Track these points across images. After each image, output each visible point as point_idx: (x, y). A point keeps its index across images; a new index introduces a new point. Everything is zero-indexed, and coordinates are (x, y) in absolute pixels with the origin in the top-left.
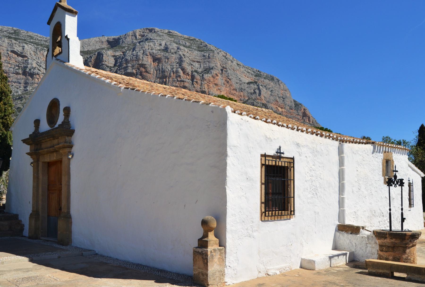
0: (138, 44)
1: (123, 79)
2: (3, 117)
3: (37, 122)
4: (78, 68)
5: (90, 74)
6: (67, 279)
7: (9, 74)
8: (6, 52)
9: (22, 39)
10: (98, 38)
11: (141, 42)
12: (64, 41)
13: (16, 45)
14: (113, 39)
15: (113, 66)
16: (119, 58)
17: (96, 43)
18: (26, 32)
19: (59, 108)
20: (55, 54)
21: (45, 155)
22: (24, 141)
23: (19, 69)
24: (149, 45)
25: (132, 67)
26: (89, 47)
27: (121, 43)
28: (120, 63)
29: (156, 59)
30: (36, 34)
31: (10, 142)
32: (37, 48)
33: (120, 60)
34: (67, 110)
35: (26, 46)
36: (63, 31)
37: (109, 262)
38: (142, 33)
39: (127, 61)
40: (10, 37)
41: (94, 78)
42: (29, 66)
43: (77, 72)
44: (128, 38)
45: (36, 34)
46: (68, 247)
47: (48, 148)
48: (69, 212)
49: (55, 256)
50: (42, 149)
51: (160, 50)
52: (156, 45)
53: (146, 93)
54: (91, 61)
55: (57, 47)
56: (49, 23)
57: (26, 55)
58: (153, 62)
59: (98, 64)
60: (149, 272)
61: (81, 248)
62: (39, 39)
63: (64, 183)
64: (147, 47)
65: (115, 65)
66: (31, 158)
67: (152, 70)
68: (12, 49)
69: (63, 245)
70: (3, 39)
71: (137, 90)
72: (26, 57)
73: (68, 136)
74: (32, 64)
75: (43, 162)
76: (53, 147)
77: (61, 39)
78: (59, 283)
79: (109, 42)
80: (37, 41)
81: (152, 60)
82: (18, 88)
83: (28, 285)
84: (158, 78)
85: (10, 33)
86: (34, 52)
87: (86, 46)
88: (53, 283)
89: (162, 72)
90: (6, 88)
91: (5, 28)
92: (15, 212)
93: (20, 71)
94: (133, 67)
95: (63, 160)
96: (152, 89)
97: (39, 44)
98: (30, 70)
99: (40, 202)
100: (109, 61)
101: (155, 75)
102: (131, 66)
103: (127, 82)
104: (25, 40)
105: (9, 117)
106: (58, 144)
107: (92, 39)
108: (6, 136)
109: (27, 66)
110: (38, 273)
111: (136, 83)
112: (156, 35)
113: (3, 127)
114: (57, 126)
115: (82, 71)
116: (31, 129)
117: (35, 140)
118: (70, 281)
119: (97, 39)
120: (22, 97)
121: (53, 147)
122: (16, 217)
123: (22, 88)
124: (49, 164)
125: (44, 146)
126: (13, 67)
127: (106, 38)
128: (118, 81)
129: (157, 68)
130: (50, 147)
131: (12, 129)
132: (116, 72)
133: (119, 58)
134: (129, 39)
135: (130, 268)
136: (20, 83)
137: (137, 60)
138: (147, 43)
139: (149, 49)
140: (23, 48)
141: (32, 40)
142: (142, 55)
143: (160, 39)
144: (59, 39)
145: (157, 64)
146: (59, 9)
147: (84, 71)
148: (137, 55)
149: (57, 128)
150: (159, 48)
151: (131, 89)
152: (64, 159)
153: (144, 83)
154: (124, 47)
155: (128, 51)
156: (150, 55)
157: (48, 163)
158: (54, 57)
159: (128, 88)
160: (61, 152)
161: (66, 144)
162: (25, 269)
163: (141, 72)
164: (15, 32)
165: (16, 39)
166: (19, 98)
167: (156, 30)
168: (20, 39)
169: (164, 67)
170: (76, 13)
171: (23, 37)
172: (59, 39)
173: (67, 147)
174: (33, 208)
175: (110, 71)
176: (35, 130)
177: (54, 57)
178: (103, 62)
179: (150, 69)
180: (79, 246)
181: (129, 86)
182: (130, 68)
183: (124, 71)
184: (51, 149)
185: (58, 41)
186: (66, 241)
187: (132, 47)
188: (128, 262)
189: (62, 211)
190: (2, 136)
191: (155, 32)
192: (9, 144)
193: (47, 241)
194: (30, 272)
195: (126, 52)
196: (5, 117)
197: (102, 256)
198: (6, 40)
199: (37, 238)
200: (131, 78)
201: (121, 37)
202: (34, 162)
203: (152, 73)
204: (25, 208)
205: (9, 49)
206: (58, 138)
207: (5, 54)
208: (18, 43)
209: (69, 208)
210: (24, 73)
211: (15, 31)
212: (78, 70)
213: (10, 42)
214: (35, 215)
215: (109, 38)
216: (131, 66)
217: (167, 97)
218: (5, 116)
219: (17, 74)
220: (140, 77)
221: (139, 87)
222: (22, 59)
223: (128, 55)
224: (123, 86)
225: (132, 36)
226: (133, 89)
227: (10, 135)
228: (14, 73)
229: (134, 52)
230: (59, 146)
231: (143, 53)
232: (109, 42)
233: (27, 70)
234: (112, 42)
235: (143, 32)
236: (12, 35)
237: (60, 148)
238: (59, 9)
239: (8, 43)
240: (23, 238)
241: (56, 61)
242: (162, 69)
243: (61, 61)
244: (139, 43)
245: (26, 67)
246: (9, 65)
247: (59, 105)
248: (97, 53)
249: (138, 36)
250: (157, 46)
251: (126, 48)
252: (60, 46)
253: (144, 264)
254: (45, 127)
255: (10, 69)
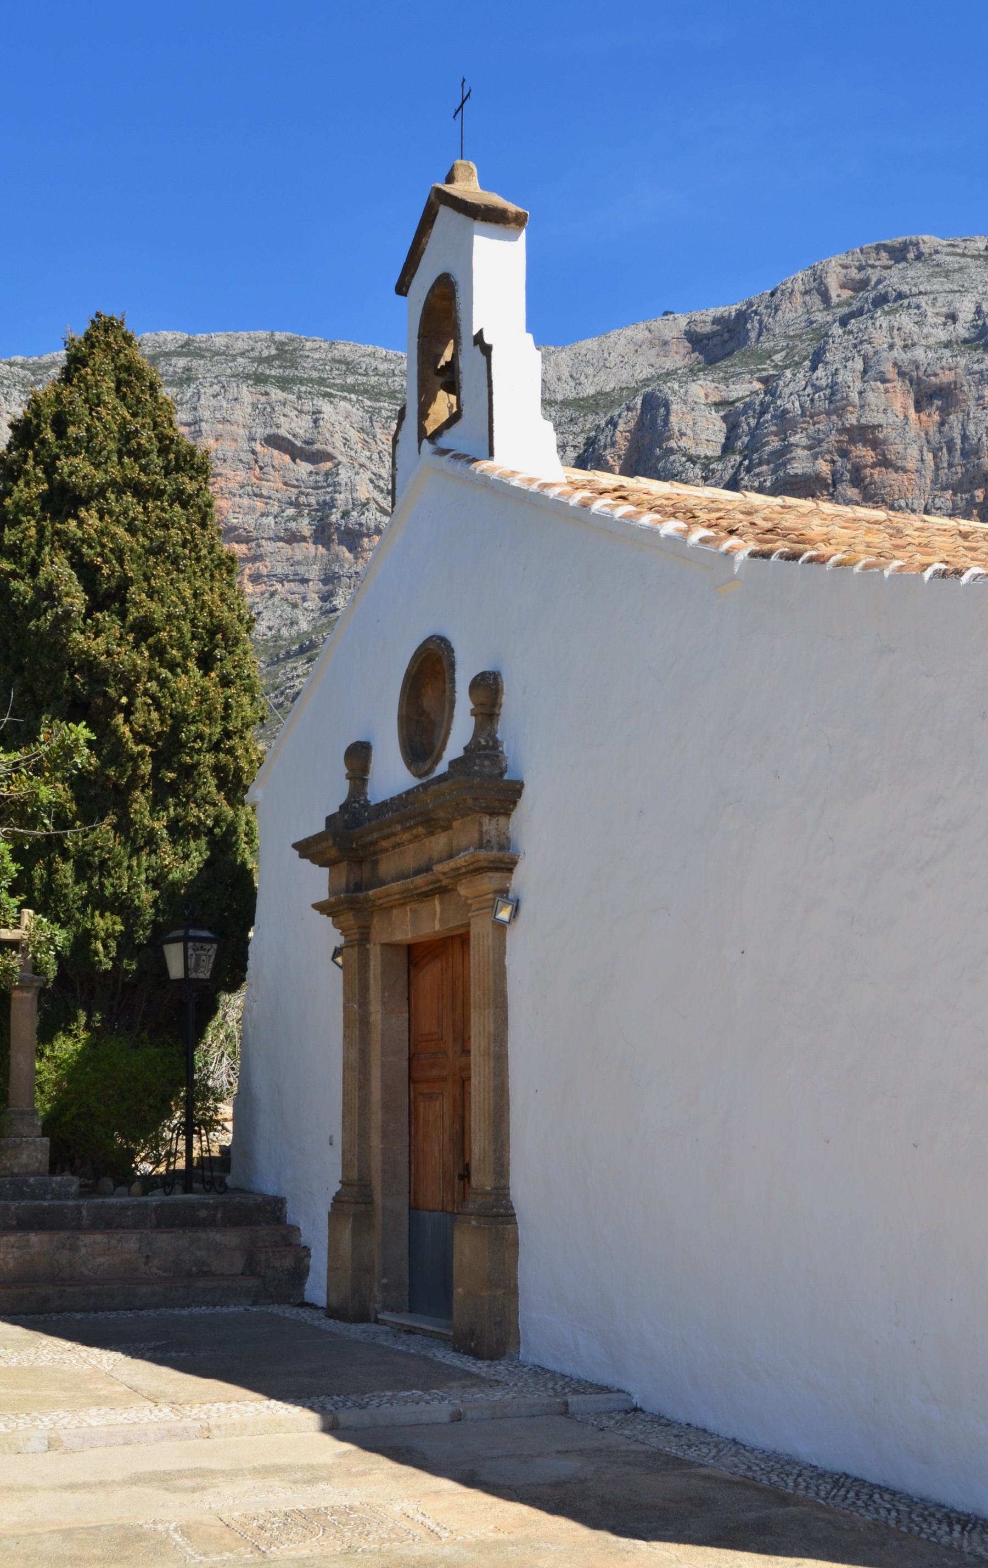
0: (837, 330)
1: (749, 513)
2: (219, 742)
3: (359, 757)
4: (531, 480)
5: (585, 505)
6: (485, 1532)
7: (259, 546)
8: (245, 446)
9: (311, 380)
10: (642, 325)
11: (853, 315)
12: (469, 361)
13: (287, 410)
14: (715, 321)
15: (718, 452)
16: (744, 412)
17: (629, 353)
18: (325, 345)
19: (453, 681)
20: (431, 427)
21: (395, 911)
22: (306, 848)
23: (300, 514)
24: (891, 328)
25: (809, 448)
26: (603, 375)
27: (753, 335)
28: (753, 433)
29: (931, 395)
30: (370, 349)
31: (247, 855)
32: (372, 413)
33: (753, 422)
34: (488, 689)
35: (326, 407)
36: (462, 315)
37: (692, 1454)
38: (854, 273)
39: (785, 422)
40: (260, 379)
41: (604, 521)
42: (340, 498)
43: (529, 502)
44: (785, 306)
45: (370, 349)
46: (501, 1367)
47: (403, 876)
48: (501, 1192)
49: (435, 1407)
50: (382, 883)
51: (947, 345)
52: (931, 319)
53: (857, 569)
54: (613, 444)
55: (442, 394)
56: (402, 288)
57: (329, 449)
58: (918, 409)
59: (648, 453)
60: (898, 1521)
61: (563, 1376)
62: (383, 367)
63: (477, 1043)
64: (880, 338)
65: (727, 448)
66: (335, 925)
67: (913, 452)
68: (269, 431)
69: (477, 1354)
70: (233, 391)
71: (811, 560)
72: (328, 457)
73: (493, 813)
74: (353, 489)
75: (383, 945)
76: (428, 869)
77: (455, 356)
78: (447, 1550)
79: (695, 340)
80: (373, 380)
81: (911, 403)
82: (295, 606)
83: (305, 1553)
84: (944, 489)
85: (261, 360)
86: (362, 430)
87: (590, 371)
88: (418, 1550)
89: (964, 454)
90: (231, 610)
91: (242, 340)
92: (270, 1189)
93: (305, 526)
94: (814, 445)
95: (474, 931)
96: (897, 547)
97: (381, 393)
98: (345, 514)
99: (376, 1141)
100: (697, 423)
101: (929, 475)
102: (805, 442)
103: (769, 525)
104: (321, 381)
105: (241, 738)
106: (451, 856)
107: (614, 334)
108: (232, 829)
109: (333, 499)
110: (355, 1491)
111: (815, 521)
112: (927, 271)
113: (219, 788)
114: (442, 768)
115: (552, 493)
116: (333, 792)
117: (350, 842)
118: (497, 1541)
119: (638, 332)
120: (313, 645)
121: (428, 869)
122: (272, 1210)
123: (314, 602)
124: (414, 956)
125: (387, 866)
126: (275, 509)
127: (683, 322)
128: (724, 523)
129: (935, 438)
130: (418, 872)
131: (256, 793)
132: (733, 485)
133: (744, 412)
134: (792, 313)
135: (801, 1493)
136: (304, 581)
137: (835, 411)
138: (882, 321)
139: (891, 347)
140: (316, 421)
141: (350, 380)
142: (858, 385)
143: (948, 286)
144: (447, 355)
145: (936, 417)
146: (445, 214)
147: (557, 490)
148: (833, 386)
149: (442, 778)
150: (943, 336)
151: (782, 556)
152: (480, 930)
153: (855, 520)
154: (769, 355)
155: (788, 373)
156: (902, 374)
157: (411, 949)
158: (425, 442)
159: (766, 555)
160: (463, 891)
161: (482, 854)
162: (302, 1468)
163: (857, 472)
164: (286, 354)
165: (284, 383)
166: (302, 650)
167: (925, 249)
168: (302, 381)
169: (971, 428)
170: (519, 220)
171: (314, 368)
172: (447, 355)
173: (490, 869)
174: (345, 1166)
175: (705, 479)
176: (351, 795)
177: (425, 442)
178: (669, 438)
179: (900, 448)
180: (552, 1365)
181: (779, 544)
182: (800, 452)
183: (774, 472)
184: (420, 880)
185: (442, 363)
186: (490, 1337)
187: (806, 347)
188: (792, 1462)
189: (473, 1183)
190: (217, 830)
191: (919, 257)
192: (244, 864)
193: (410, 1331)
194: (322, 1486)
195: (779, 377)
196: (229, 743)
197: (662, 1422)
198: (246, 393)
199: (362, 1316)
200: (790, 501)
201: (750, 304)
202: (348, 945)
203: (911, 464)
204: (310, 1169)
205: (260, 432)
206: (447, 828)
207: (243, 456)
208: (293, 397)
209: (501, 1169)
210: (322, 534)
211: (281, 346)
212: (534, 488)
213: (263, 399)
214: (353, 1201)
215: (698, 317)
216: (805, 442)
217: (965, 579)
218: (227, 734)
219: (293, 538)
220: (852, 493)
221: (827, 541)
222: (310, 467)
223: (787, 391)
224: (742, 547)
225: (807, 292)
226: (794, 556)
227: (247, 823)
228: (281, 539)
229: (820, 372)
230: (452, 864)
231: (865, 372)
232: (695, 340)
233: (333, 518)
234: (709, 336)
235: (861, 268)
236: (271, 367)
237: (458, 875)
238: (445, 214)
239: (254, 406)
240: (304, 1314)
241: (436, 457)
242: (965, 438)
243: (458, 457)
244: (844, 322)
245: (328, 505)
246: (259, 504)
247: (452, 666)
248: (639, 401)
249: (835, 292)
250: (934, 326)
251: (778, 357)
252: (452, 387)
253: (873, 1476)
254: (391, 776)
255: (265, 520)
